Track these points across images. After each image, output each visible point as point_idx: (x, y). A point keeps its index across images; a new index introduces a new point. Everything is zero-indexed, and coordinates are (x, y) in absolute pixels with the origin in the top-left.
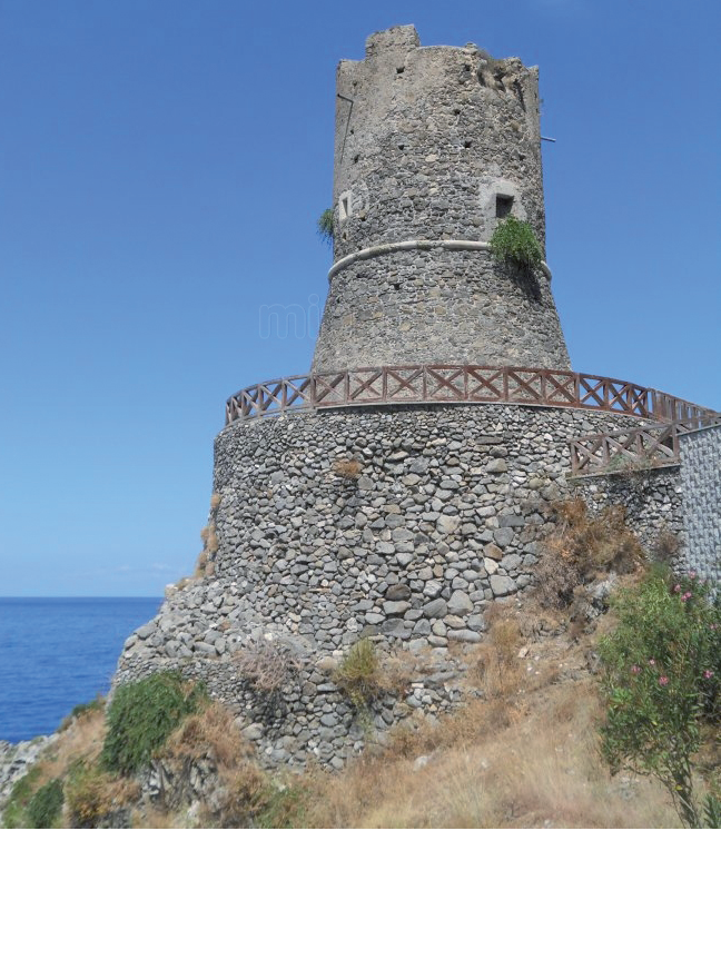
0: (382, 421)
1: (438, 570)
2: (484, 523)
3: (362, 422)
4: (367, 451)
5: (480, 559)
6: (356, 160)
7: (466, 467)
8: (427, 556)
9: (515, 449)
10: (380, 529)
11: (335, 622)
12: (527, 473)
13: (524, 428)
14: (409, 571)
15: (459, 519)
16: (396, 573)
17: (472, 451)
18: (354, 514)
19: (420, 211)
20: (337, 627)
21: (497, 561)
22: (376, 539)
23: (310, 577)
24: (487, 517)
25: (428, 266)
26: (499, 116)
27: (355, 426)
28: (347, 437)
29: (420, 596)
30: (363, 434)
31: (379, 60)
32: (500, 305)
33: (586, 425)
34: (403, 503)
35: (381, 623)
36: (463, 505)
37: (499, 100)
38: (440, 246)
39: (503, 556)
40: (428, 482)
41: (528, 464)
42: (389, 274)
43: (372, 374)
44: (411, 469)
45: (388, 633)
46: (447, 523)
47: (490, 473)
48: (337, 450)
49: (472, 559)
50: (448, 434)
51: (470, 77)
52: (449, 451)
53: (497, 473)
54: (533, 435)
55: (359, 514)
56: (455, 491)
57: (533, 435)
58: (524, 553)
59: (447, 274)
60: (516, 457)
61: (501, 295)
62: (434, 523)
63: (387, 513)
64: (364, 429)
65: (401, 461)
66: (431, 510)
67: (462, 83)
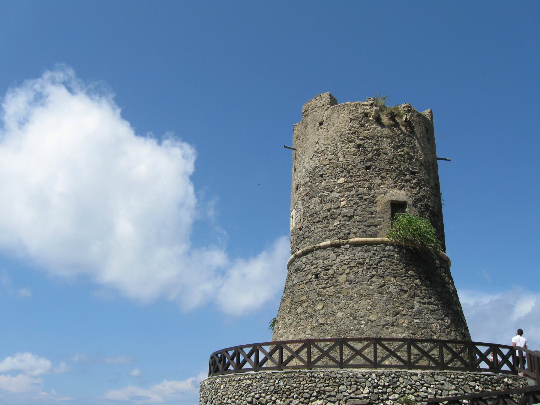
3: (263, 386)
13: (389, 390)
26: (392, 145)
28: (253, 397)
30: (263, 395)
31: (309, 119)
33: (447, 386)
37: (391, 134)
38: (347, 243)
42: (313, 267)
50: (324, 397)
51: (368, 121)
54: (397, 396)
61: (395, 277)
67: (362, 125)
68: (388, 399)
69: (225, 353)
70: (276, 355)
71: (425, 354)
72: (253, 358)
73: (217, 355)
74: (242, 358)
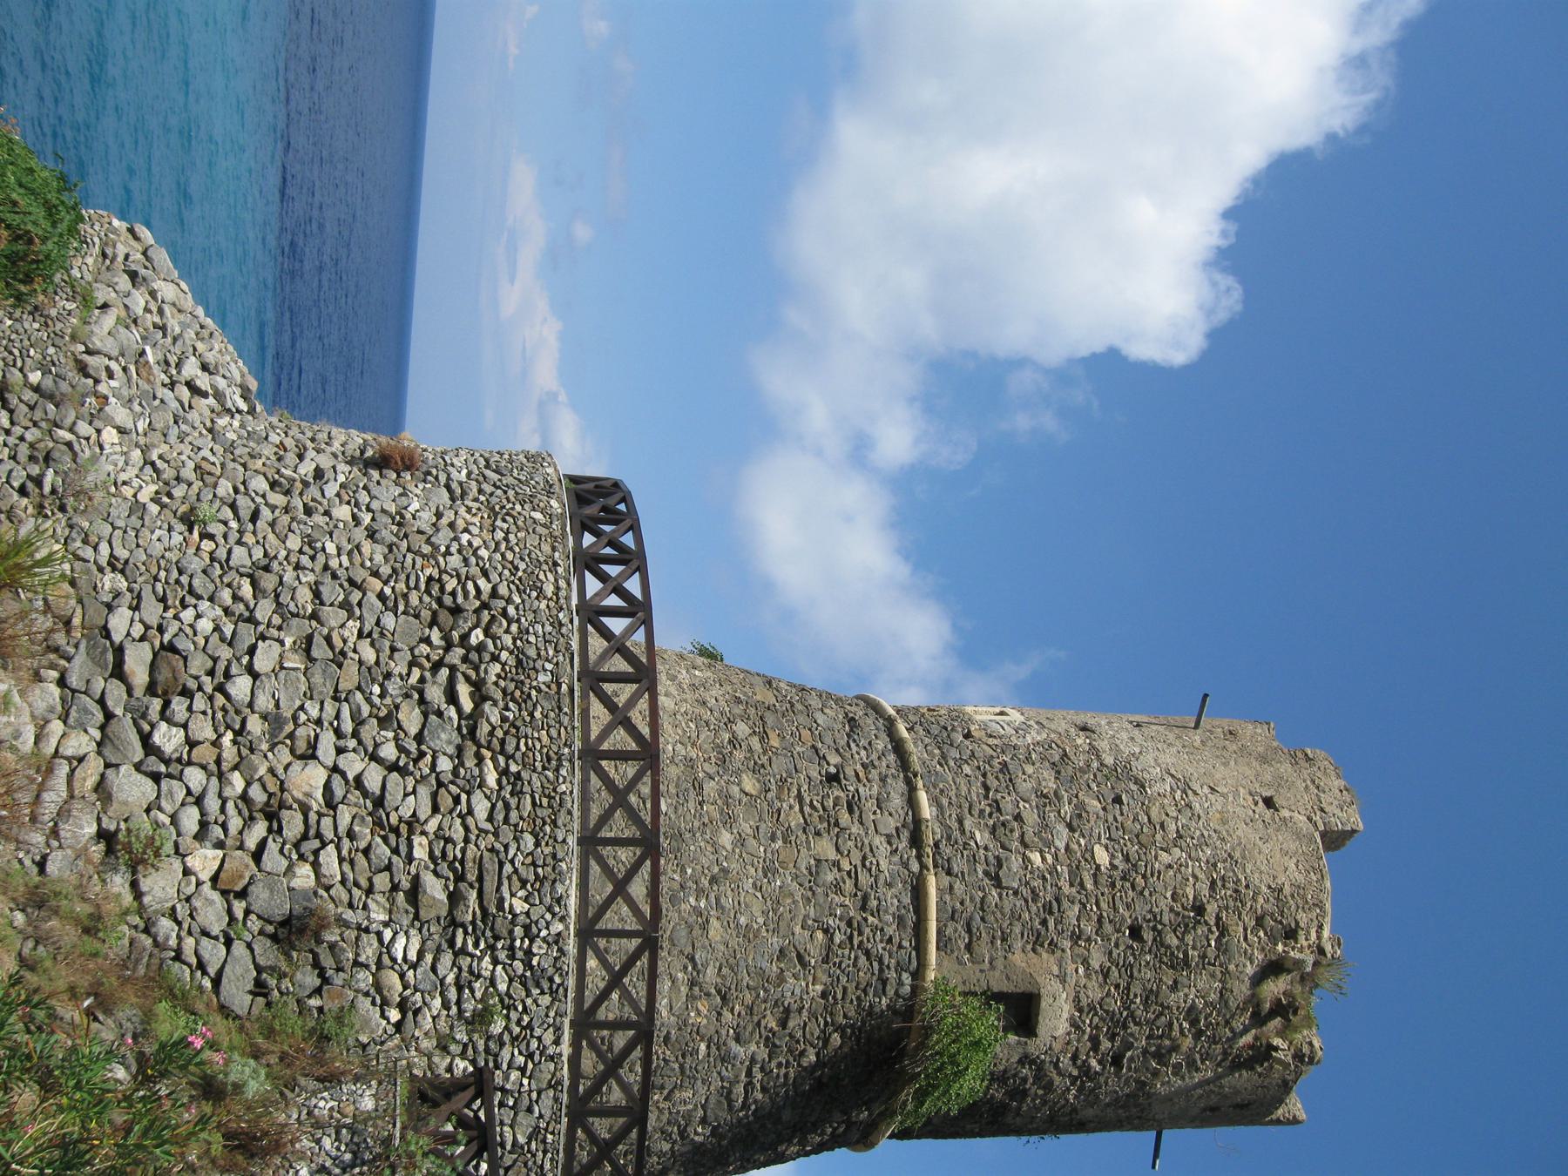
0: (539, 664)
1: (205, 753)
2: (301, 857)
3: (539, 628)
4: (477, 636)
5: (220, 845)
6: (1084, 729)
7: (432, 826)
8: (238, 733)
9: (470, 942)
10: (308, 651)
11: (122, 554)
12: (414, 966)
13: (518, 965)
14: (211, 698)
15: (315, 807)
16: (211, 673)
17: (466, 840)
18: (345, 605)
19: (993, 831)
20: (111, 555)
21: (215, 879)
22: (288, 641)
23: (225, 523)
24: (316, 865)
25: (878, 841)
26: (1200, 1003)
27: (531, 617)
28: (509, 601)
29: (154, 713)
31: (1285, 768)
32: (802, 988)
34: (359, 695)
35: (108, 636)
36: (345, 816)
37: (1233, 1004)
38: (923, 866)
39: (224, 893)
40: (401, 749)
41: (434, 969)
43: (645, 731)
44: (433, 718)
45: (83, 646)
46: (310, 780)
47: (416, 881)
48: (482, 582)
49: (224, 826)
50: (506, 793)
52: (469, 793)
53: (414, 893)
54: (503, 987)
55: (343, 614)
56: (379, 802)
57: (503, 987)
58: (228, 943)
59: (864, 878)
60: (451, 943)
61: (824, 995)
62: (310, 755)
63: (340, 666)
64: (524, 632)
65: (452, 698)
66: (340, 751)
67: (1260, 921)
68: (495, 962)
69: (628, 523)
70: (619, 664)
71: (612, 1068)
72: (614, 601)
73: (623, 500)
74: (613, 570)
